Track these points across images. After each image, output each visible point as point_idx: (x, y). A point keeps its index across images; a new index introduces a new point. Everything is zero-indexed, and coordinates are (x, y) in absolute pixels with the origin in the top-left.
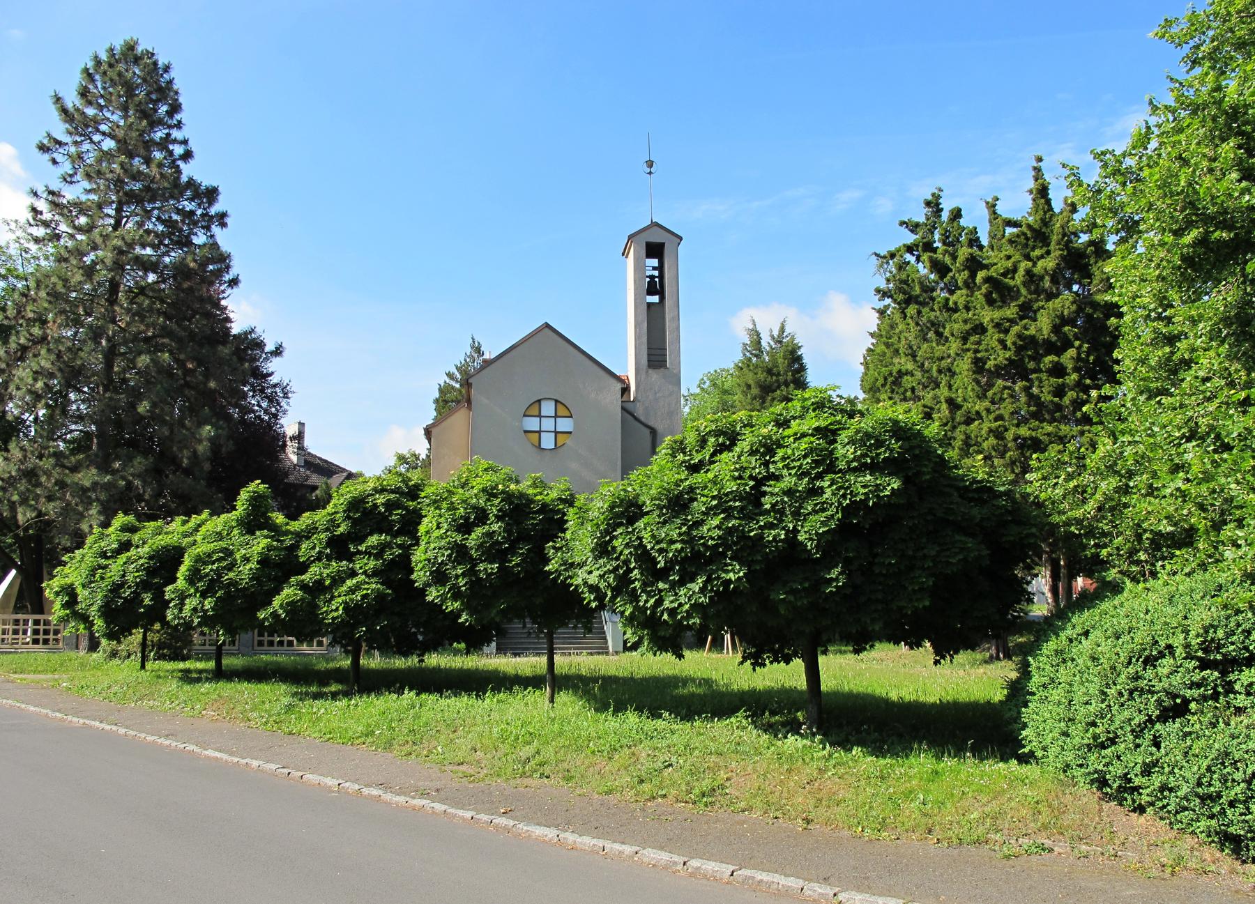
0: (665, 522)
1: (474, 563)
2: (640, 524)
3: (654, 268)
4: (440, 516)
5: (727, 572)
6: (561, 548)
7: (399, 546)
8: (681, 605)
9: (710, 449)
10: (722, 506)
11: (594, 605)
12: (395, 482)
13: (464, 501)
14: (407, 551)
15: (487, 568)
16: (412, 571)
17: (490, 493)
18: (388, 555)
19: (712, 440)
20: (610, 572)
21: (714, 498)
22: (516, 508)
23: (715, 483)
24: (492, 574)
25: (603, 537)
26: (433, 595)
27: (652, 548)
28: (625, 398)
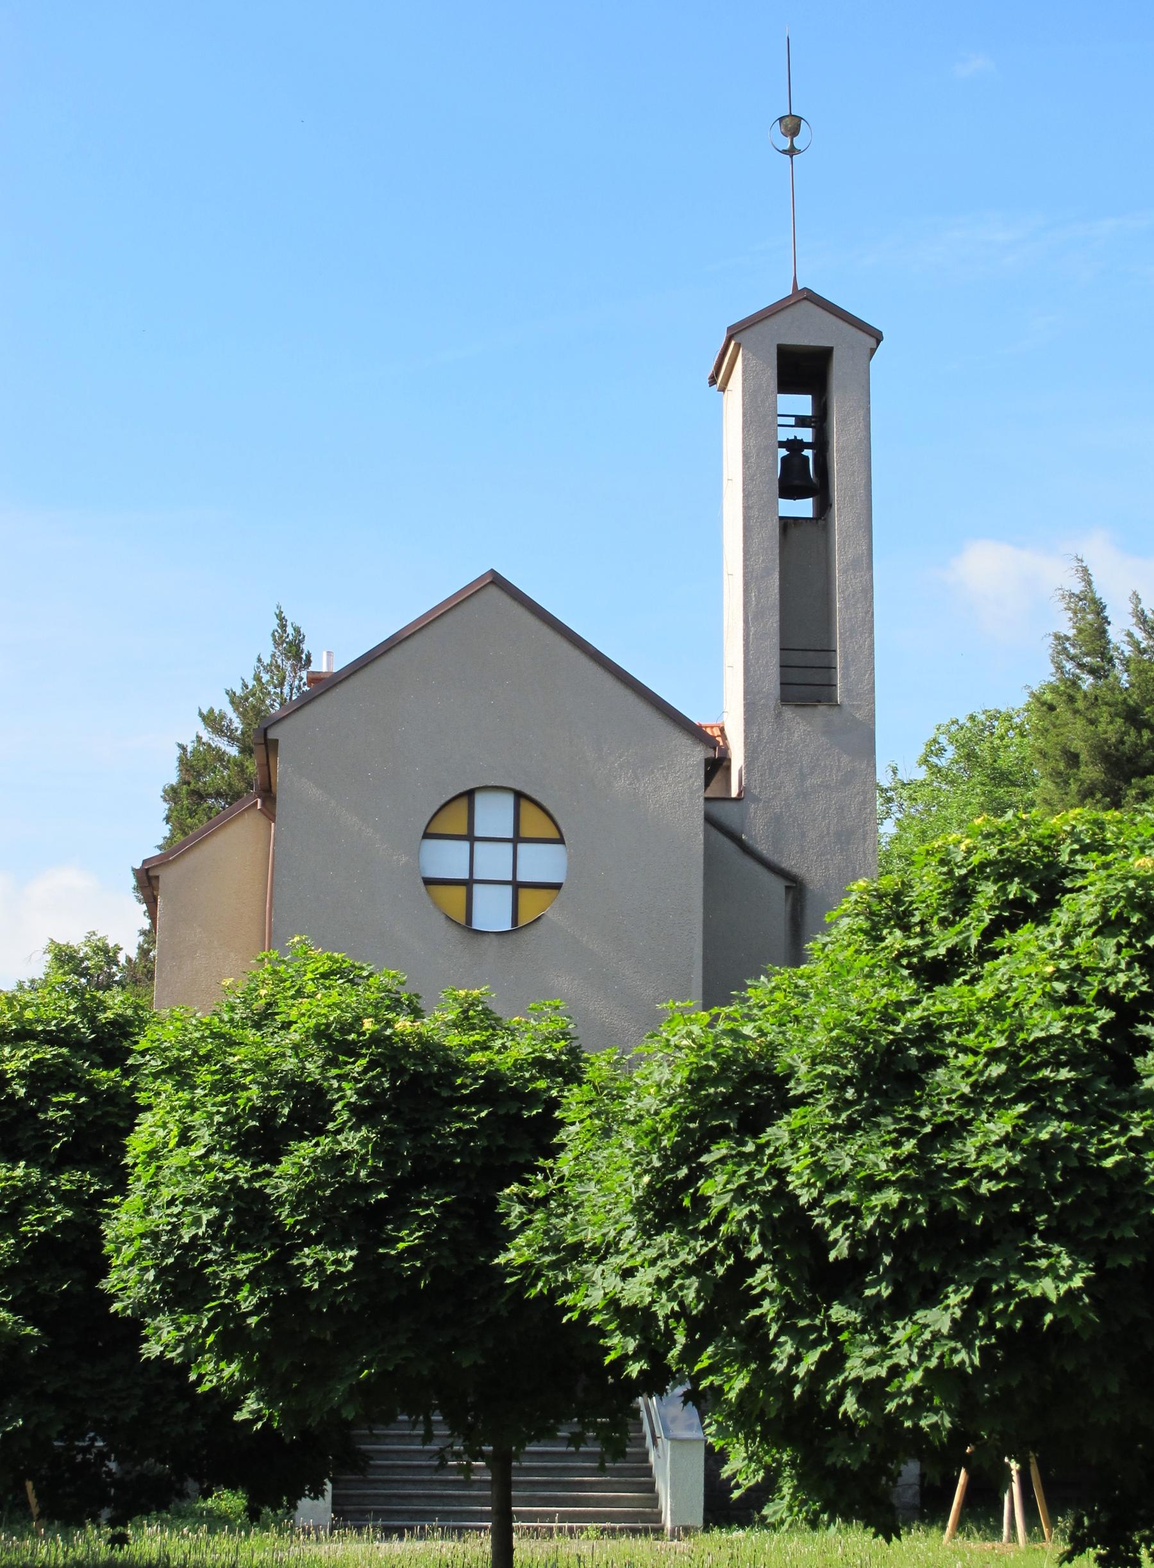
0: (851, 1127)
1: (286, 1244)
2: (778, 1132)
3: (801, 422)
4: (192, 1107)
5: (1034, 1274)
6: (543, 1202)
7: (66, 1198)
8: (896, 1371)
9: (981, 914)
10: (1020, 1077)
11: (634, 1369)
12: (59, 1010)
13: (263, 1065)
14: (90, 1211)
15: (324, 1260)
16: (103, 1267)
17: (336, 1042)
18: (31, 1225)
19: (988, 889)
20: (688, 1270)
21: (994, 1055)
22: (414, 1088)
23: (998, 1014)
24: (337, 1277)
25: (668, 1168)
26: (162, 1339)
27: (815, 1203)
28: (715, 790)
